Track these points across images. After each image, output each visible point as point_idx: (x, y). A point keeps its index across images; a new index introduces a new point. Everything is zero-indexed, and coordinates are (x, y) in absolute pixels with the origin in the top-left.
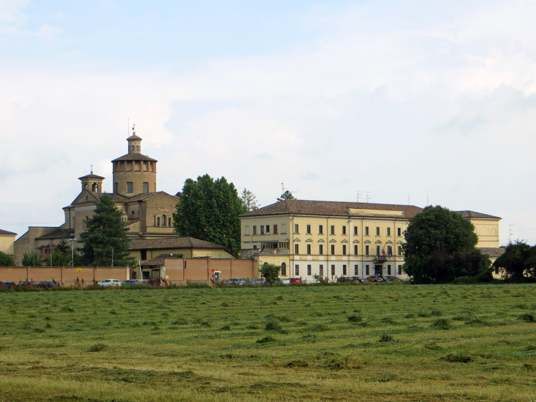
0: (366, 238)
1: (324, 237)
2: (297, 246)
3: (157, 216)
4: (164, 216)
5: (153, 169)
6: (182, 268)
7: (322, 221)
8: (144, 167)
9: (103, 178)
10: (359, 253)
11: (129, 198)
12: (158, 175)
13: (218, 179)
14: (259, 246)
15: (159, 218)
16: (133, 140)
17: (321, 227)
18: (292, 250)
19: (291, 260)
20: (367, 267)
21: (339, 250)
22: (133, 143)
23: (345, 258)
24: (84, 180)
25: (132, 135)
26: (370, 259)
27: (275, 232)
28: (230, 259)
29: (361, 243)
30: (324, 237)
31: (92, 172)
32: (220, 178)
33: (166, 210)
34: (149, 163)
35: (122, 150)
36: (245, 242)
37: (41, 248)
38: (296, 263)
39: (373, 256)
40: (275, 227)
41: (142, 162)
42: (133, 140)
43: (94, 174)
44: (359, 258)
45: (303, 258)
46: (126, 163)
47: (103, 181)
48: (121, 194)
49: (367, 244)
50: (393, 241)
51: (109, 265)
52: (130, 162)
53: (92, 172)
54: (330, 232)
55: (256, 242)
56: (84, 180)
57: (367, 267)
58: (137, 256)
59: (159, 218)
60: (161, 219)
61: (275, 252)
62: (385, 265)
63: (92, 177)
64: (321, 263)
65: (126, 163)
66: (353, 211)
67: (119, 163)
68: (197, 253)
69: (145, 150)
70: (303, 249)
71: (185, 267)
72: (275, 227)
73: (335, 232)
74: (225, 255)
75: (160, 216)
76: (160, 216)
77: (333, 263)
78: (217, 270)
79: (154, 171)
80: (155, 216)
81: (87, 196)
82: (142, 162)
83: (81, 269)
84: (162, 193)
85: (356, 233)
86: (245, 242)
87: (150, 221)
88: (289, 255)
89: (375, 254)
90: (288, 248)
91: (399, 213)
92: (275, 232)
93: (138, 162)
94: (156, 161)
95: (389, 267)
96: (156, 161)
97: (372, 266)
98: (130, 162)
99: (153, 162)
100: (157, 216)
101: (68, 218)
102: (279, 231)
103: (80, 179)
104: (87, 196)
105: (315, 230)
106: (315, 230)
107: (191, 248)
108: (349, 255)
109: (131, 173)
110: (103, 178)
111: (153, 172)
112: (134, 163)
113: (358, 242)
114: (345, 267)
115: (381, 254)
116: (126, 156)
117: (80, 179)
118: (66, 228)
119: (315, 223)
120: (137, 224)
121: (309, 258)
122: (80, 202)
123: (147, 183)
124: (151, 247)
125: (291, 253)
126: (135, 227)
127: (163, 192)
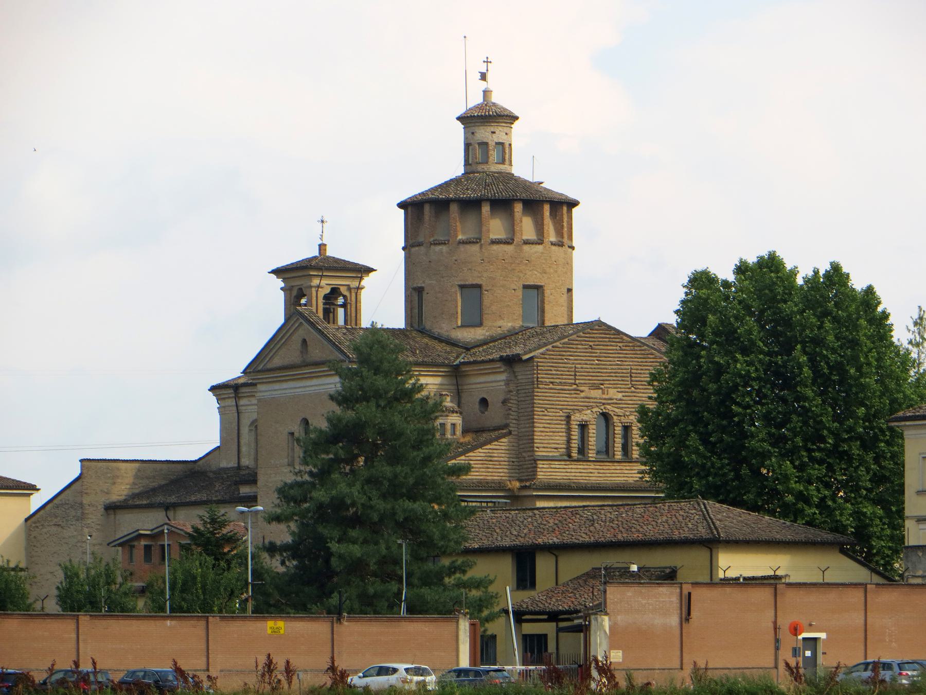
3: (577, 418)
5: (559, 232)
6: (674, 620)
8: (526, 227)
11: (467, 348)
12: (579, 258)
15: (583, 427)
16: (484, 122)
22: (483, 133)
24: (294, 277)
31: (322, 247)
33: (613, 393)
34: (547, 208)
41: (518, 208)
42: (484, 122)
43: (330, 252)
47: (367, 281)
48: (436, 331)
52: (471, 205)
53: (322, 247)
56: (294, 277)
58: (502, 571)
59: (583, 427)
60: (592, 431)
63: (323, 264)
71: (686, 615)
76: (587, 415)
78: (811, 627)
79: (564, 240)
80: (568, 417)
82: (518, 208)
83: (281, 624)
84: (599, 328)
87: (549, 437)
93: (502, 205)
94: (573, 204)
96: (573, 204)
99: (563, 206)
100: (577, 418)
103: (277, 272)
109: (475, 248)
111: (560, 244)
116: (456, 181)
117: (277, 272)
118: (224, 464)
120: (500, 449)
122: (277, 362)
123: (538, 288)
124: (554, 539)
126: (489, 459)
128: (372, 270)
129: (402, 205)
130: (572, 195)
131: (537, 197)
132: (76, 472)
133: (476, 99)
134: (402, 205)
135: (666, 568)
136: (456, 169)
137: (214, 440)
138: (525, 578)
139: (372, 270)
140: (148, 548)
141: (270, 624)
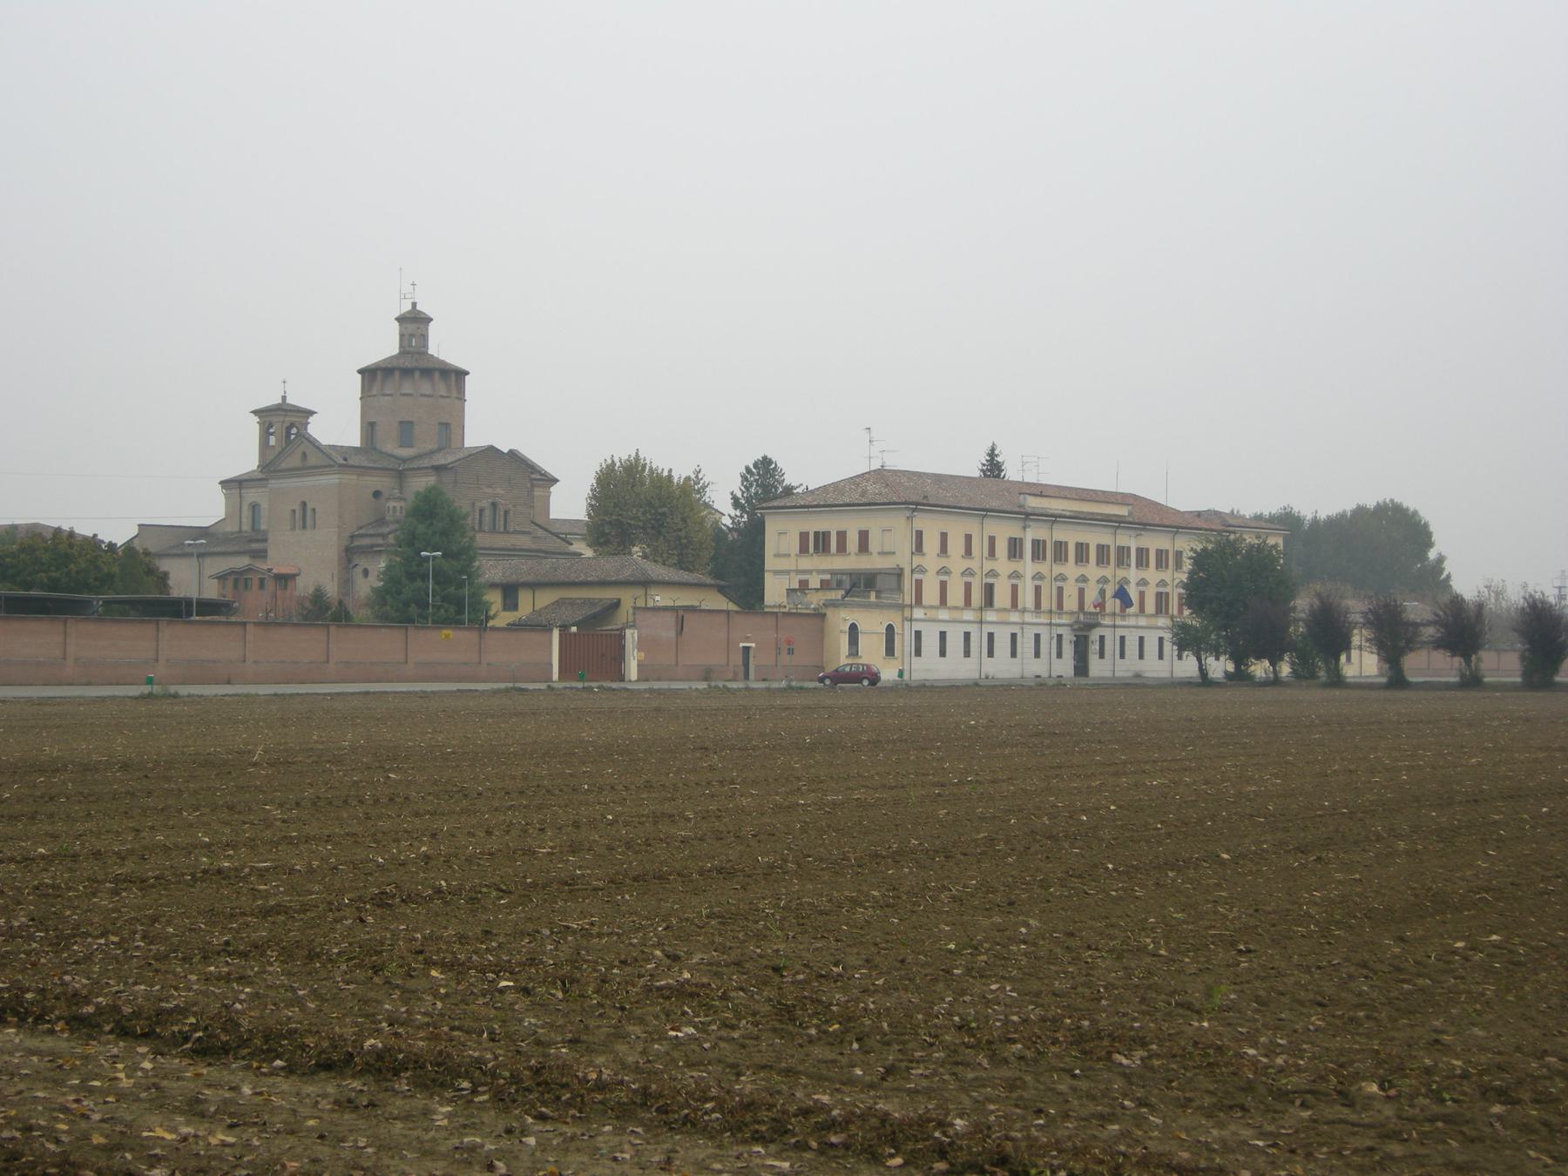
0: (988, 565)
1: (974, 564)
2: (919, 583)
3: (478, 505)
4: (494, 505)
6: (672, 634)
7: (971, 526)
8: (441, 389)
9: (312, 413)
10: (1045, 605)
11: (404, 461)
12: (469, 407)
13: (283, 425)
14: (815, 582)
15: (481, 511)
16: (414, 323)
17: (968, 538)
18: (908, 597)
19: (904, 619)
20: (1060, 637)
21: (1002, 596)
23: (1014, 617)
24: (267, 416)
25: (409, 308)
26: (1065, 620)
27: (864, 547)
28: (728, 612)
29: (978, 578)
30: (974, 564)
31: (284, 398)
32: (253, 426)
33: (499, 491)
35: (385, 345)
36: (776, 572)
37: (222, 578)
38: (917, 626)
39: (1072, 613)
40: (864, 536)
41: (437, 375)
42: (414, 323)
44: (1044, 619)
45: (932, 614)
46: (397, 374)
49: (1060, 584)
50: (977, 570)
51: (462, 622)
52: (407, 372)
53: (284, 398)
54: (986, 553)
55: (810, 572)
56: (267, 416)
57: (1060, 637)
58: (494, 599)
59: (481, 511)
60: (487, 513)
61: (873, 597)
62: (1095, 635)
64: (968, 628)
65: (397, 374)
66: (1033, 503)
67: (379, 375)
68: (660, 598)
69: (442, 346)
70: (931, 595)
71: (680, 629)
72: (864, 536)
73: (926, 548)
74: (717, 602)
75: (485, 504)
76: (485, 504)
77: (991, 629)
78: (747, 639)
81: (304, 454)
82: (437, 375)
83: (449, 632)
84: (491, 452)
85: (968, 552)
86: (776, 572)
88: (902, 607)
89: (1075, 608)
90: (900, 589)
91: (1122, 511)
92: (864, 547)
95: (1102, 638)
97: (1068, 637)
98: (407, 372)
100: (478, 505)
101: (233, 510)
102: (874, 545)
103: (255, 412)
104: (304, 454)
105: (956, 546)
106: (956, 546)
107: (646, 583)
108: (1024, 611)
110: (312, 413)
112: (417, 374)
113: (972, 574)
114: (1014, 636)
115: (1089, 607)
117: (255, 412)
118: (228, 529)
119: (957, 529)
121: (943, 614)
122: (284, 466)
123: (447, 425)
124: (531, 578)
125: (907, 601)
127: (491, 449)
128: (992, 454)
129: (360, 372)
130: (461, 364)
131: (431, 365)
132: (135, 531)
133: (407, 307)
134: (360, 372)
135: (877, 606)
136: (394, 350)
137: (221, 514)
138: (511, 603)
139: (992, 454)
140: (236, 581)
141: (445, 632)
